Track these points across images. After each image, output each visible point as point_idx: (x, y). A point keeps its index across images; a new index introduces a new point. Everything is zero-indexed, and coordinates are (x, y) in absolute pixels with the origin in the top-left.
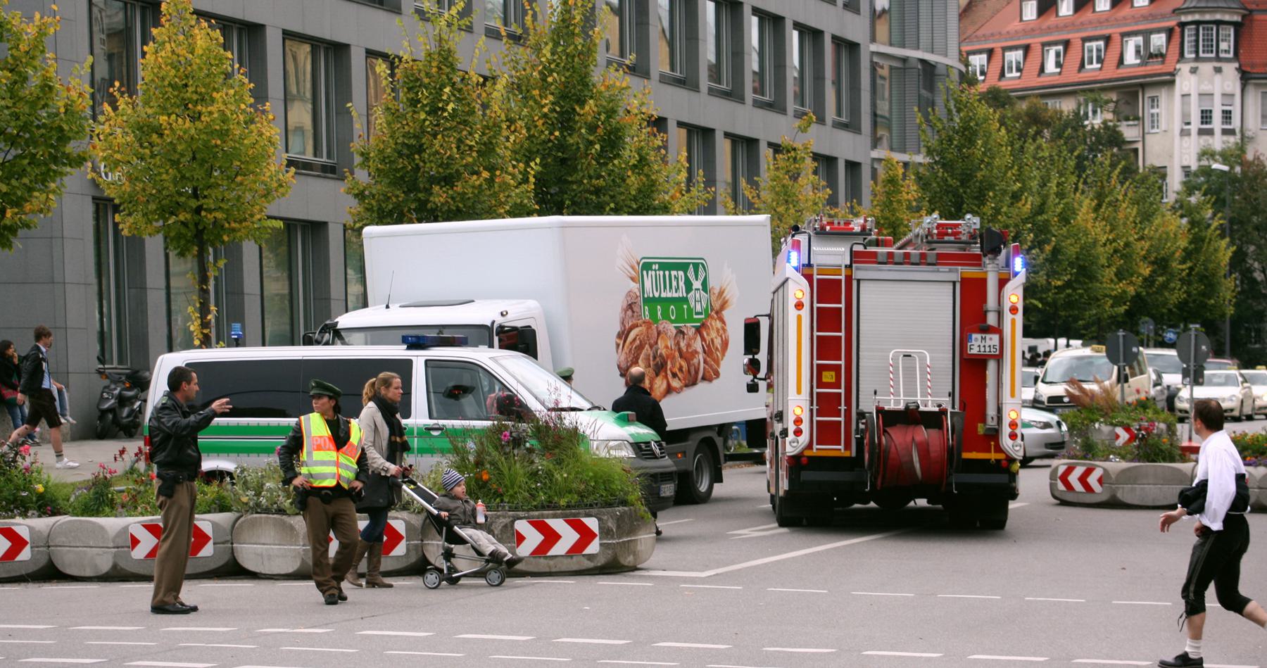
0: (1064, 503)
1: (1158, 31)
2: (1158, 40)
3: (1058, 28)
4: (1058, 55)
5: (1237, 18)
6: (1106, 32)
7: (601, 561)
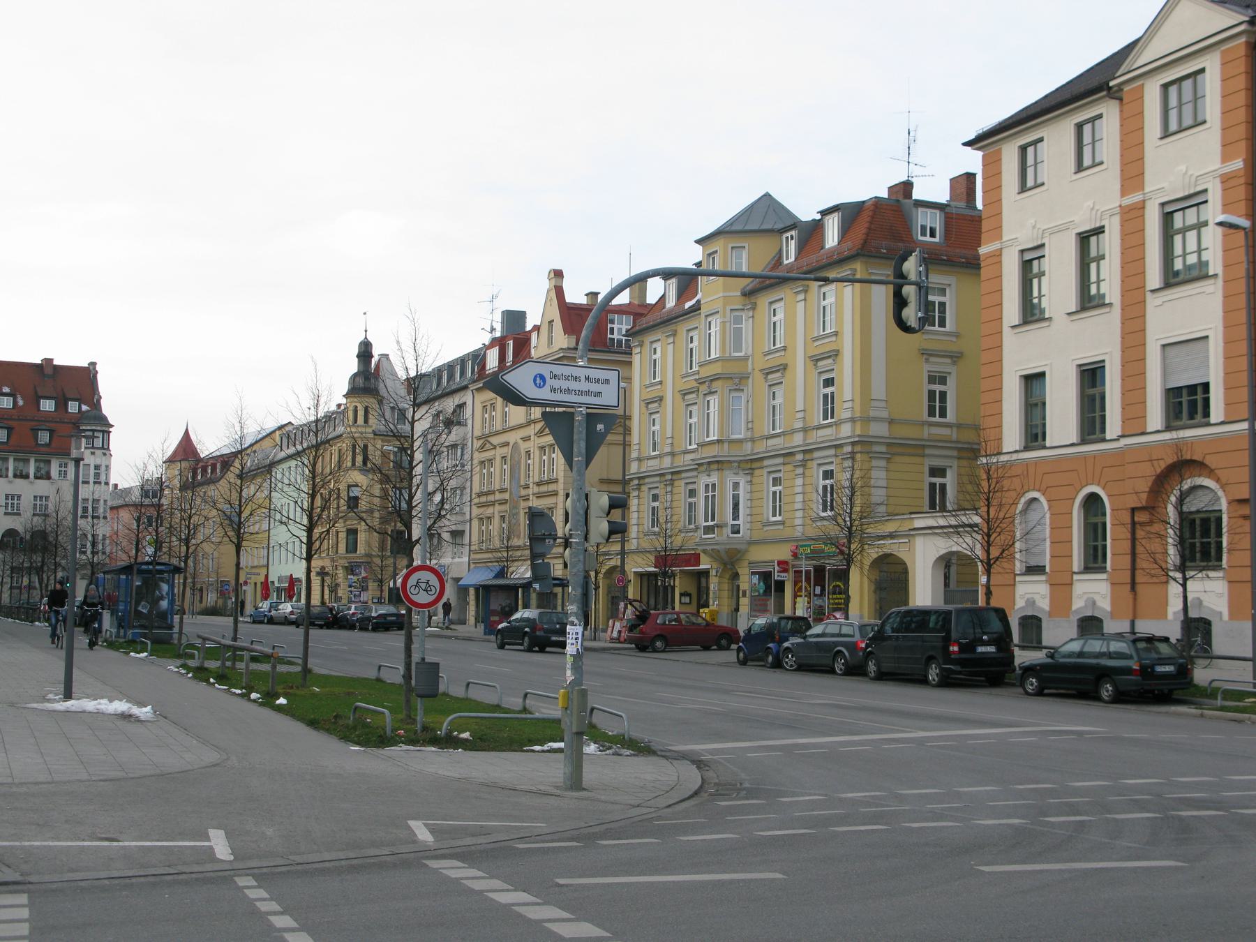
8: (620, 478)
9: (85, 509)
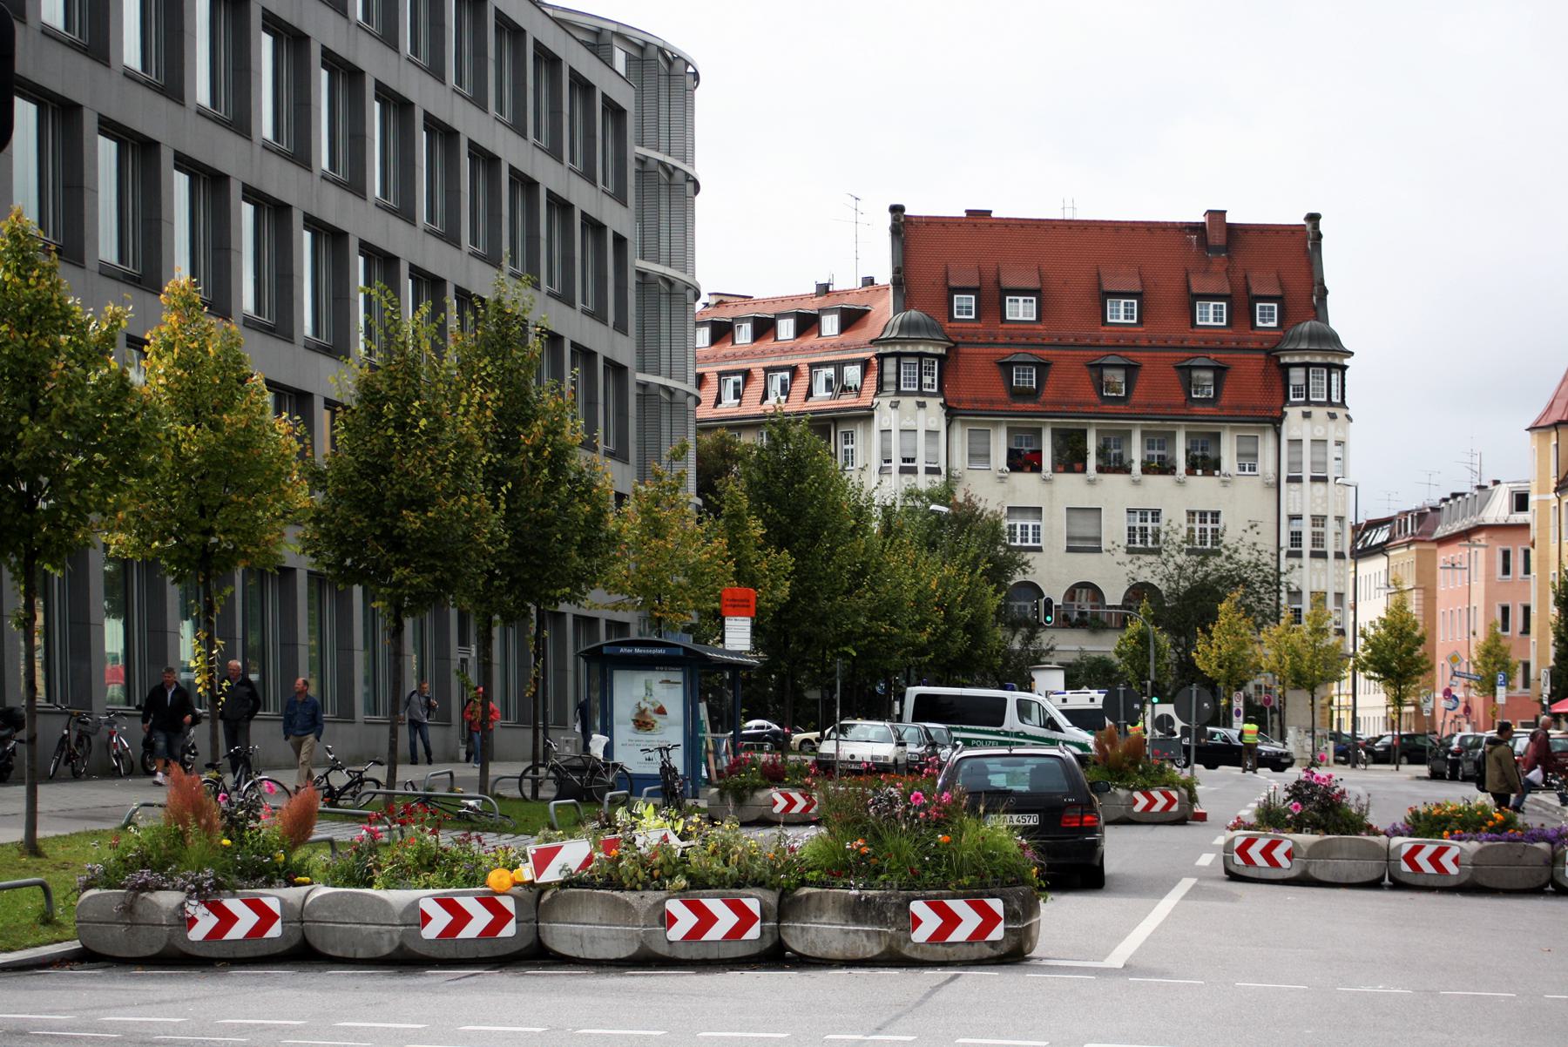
0: (1233, 877)
1: (853, 362)
2: (852, 374)
3: (735, 357)
4: (736, 384)
5: (941, 351)
6: (792, 362)
7: (1005, 949)
8: (42, 790)
9: (1296, 538)
